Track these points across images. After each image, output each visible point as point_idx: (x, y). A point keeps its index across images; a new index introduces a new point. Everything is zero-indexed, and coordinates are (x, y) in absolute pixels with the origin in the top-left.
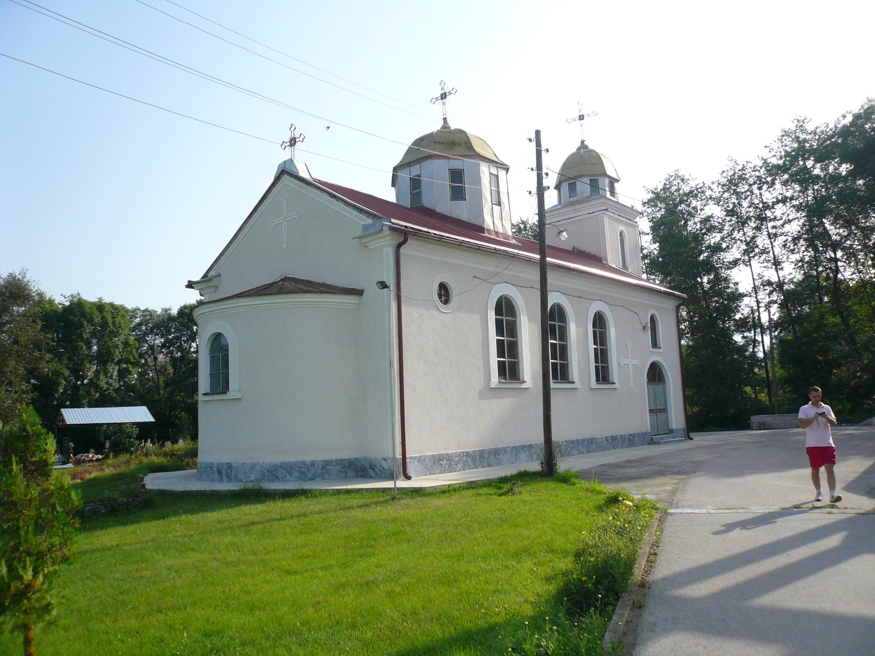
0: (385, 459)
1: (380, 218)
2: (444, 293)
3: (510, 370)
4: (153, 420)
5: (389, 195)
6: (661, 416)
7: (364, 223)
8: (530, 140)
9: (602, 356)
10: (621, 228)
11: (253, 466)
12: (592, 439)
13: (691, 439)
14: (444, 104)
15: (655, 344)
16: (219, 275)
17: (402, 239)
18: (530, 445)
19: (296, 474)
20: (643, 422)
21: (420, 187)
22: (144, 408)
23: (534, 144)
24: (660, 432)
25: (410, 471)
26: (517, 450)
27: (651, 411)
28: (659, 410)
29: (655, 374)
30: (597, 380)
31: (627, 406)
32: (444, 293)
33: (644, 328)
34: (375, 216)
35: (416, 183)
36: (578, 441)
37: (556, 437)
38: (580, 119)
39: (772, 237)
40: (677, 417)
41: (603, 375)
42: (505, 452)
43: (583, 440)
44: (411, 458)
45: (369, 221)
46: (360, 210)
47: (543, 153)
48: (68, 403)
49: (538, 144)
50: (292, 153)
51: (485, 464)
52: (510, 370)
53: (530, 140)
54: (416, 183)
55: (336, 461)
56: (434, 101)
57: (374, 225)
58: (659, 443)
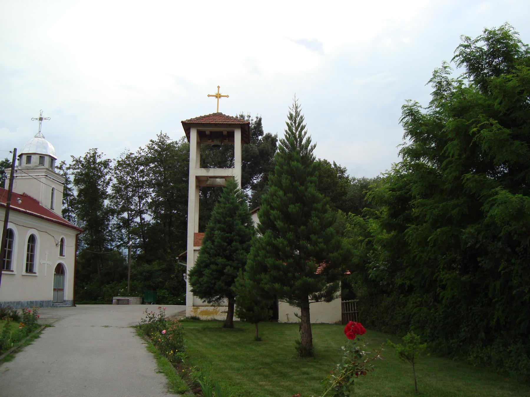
6: (60, 293)
9: (30, 258)
12: (19, 302)
15: (61, 254)
20: (49, 295)
23: (12, 155)
24: (57, 303)
27: (54, 290)
28: (59, 289)
29: (60, 270)
30: (27, 271)
33: (57, 245)
36: (11, 302)
38: (40, 120)
39: (141, 198)
40: (69, 293)
41: (30, 268)
43: (14, 302)
44: (314, 324)
48: (20, 202)
58: (57, 307)
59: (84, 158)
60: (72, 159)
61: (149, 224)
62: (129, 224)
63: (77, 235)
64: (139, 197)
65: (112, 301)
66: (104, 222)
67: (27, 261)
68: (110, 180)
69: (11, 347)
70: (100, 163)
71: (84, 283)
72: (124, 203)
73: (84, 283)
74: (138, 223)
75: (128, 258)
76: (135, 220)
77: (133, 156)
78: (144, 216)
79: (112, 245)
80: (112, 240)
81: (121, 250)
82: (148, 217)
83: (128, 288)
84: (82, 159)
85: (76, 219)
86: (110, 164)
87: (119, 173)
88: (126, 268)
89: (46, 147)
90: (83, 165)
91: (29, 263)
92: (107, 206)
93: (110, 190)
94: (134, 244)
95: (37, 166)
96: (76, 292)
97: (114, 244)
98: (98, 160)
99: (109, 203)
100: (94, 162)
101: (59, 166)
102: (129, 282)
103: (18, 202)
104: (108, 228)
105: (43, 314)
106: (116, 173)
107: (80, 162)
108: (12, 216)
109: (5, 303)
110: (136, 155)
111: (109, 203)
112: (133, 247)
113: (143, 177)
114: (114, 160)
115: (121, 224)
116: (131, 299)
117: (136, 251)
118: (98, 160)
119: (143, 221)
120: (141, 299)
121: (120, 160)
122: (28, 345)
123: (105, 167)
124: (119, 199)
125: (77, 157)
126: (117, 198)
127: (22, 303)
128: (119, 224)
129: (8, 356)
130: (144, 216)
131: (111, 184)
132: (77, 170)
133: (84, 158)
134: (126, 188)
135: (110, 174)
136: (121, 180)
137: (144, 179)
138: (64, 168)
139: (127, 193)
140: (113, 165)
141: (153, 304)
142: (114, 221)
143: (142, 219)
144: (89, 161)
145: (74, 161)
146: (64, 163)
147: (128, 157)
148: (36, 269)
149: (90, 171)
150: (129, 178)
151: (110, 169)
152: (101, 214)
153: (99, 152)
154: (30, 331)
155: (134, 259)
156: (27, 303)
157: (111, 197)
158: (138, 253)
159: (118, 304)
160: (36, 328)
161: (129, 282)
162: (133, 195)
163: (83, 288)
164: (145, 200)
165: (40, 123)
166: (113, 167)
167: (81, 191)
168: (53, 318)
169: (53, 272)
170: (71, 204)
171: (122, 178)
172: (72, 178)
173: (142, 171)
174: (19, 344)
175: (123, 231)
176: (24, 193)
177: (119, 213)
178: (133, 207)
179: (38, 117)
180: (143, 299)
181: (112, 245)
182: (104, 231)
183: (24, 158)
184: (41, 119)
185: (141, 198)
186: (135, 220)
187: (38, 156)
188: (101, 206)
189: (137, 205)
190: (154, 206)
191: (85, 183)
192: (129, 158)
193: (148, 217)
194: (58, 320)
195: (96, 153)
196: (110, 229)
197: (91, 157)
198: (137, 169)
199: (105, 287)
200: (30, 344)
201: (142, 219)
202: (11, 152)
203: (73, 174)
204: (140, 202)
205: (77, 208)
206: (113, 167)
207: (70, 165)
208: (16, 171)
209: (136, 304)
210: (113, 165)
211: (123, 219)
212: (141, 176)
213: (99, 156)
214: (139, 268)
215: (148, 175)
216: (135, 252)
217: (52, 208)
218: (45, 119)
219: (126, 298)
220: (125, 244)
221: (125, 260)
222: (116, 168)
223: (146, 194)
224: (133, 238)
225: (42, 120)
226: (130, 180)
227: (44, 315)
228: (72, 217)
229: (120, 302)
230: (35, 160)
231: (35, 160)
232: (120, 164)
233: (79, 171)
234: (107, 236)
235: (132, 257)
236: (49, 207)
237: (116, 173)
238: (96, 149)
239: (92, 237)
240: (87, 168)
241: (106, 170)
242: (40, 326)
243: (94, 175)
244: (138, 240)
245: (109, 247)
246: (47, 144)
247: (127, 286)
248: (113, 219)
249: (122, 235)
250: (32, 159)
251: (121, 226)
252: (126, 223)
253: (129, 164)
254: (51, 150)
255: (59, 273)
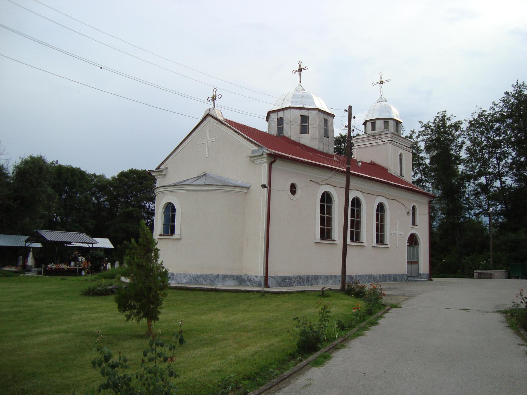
0: (256, 277)
1: (262, 147)
2: (293, 189)
3: (326, 234)
4: (113, 247)
5: (263, 126)
6: (414, 266)
7: (253, 149)
8: (346, 111)
10: (401, 151)
11: (185, 275)
13: (432, 280)
14: (300, 75)
15: (414, 223)
16: (167, 169)
17: (273, 160)
18: (335, 276)
19: (208, 281)
20: (402, 268)
21: (282, 124)
22: (107, 239)
23: (347, 113)
24: (412, 276)
25: (270, 283)
26: (327, 278)
27: (408, 262)
28: (413, 261)
29: (413, 240)
30: (377, 242)
31: (392, 259)
32: (293, 189)
33: (408, 213)
34: (259, 146)
35: (281, 121)
36: (363, 275)
37: (348, 273)
39: (499, 159)
40: (424, 266)
41: (380, 239)
42: (321, 278)
44: (270, 277)
45: (256, 148)
46: (251, 142)
47: (352, 119)
49: (350, 114)
50: (214, 105)
51: (309, 284)
52: (326, 234)
53: (346, 111)
54: (281, 121)
55: (230, 275)
56: (294, 72)
57: (258, 150)
58: (411, 281)
59: (433, 123)
60: (420, 125)
61: (511, 188)
62: (488, 189)
63: (430, 203)
64: (497, 159)
65: (473, 275)
66: (460, 189)
67: (377, 231)
68: (463, 143)
69: (335, 339)
70: (451, 126)
71: (442, 255)
72: (481, 167)
73: (442, 255)
74: (497, 187)
75: (489, 227)
76: (494, 185)
77: (486, 113)
78: (505, 179)
79: (470, 214)
80: (471, 208)
81: (480, 219)
82: (509, 181)
83: (491, 260)
84: (431, 124)
85: (430, 189)
86: (462, 126)
87: (472, 134)
88: (487, 238)
89: (389, 110)
90: (432, 130)
91: (379, 233)
92: (462, 172)
93: (463, 154)
94: (495, 210)
95: (382, 132)
96: (432, 264)
97: (472, 212)
98: (448, 123)
99: (464, 168)
100: (444, 125)
101: (409, 136)
102: (491, 253)
103: (357, 165)
104: (464, 195)
105: (390, 289)
106: (468, 135)
107: (430, 127)
108: (353, 182)
109: (356, 276)
110: (489, 112)
111: (464, 168)
112: (494, 214)
113: (501, 136)
114: (465, 120)
115: (479, 190)
116: (495, 272)
117: (498, 218)
118: (448, 123)
119: (504, 185)
120: (507, 273)
121: (472, 119)
122: (358, 335)
123: (457, 130)
124: (475, 162)
125: (425, 122)
126: (472, 162)
127: (374, 276)
128: (477, 190)
129: (321, 356)
130: (505, 179)
131: (464, 147)
132: (427, 136)
133: (433, 123)
134: (482, 149)
135: (462, 136)
136: (474, 141)
137: (501, 138)
138: (414, 137)
139: (482, 155)
140: (464, 126)
141: (522, 278)
142: (470, 187)
143: (502, 183)
144: (438, 125)
145: (422, 127)
146: (413, 132)
147: (480, 116)
148: (387, 240)
149: (441, 134)
150: (483, 139)
151: (462, 131)
152: (456, 181)
153: (448, 115)
154: (370, 312)
155: (496, 227)
156: (380, 276)
157: (466, 162)
158: (500, 220)
159: (480, 277)
160: (380, 308)
161: (491, 253)
162: (490, 157)
163: (441, 260)
164: (504, 161)
165: (381, 87)
166: (465, 129)
167: (432, 159)
168: (404, 296)
169: (406, 243)
170: (424, 172)
171: (475, 139)
172: (422, 145)
173: (498, 129)
174: (349, 333)
175: (482, 197)
176: (372, 161)
177: (476, 178)
178: (491, 170)
179: (378, 81)
180: (509, 273)
181: (470, 214)
182: (461, 198)
183: (369, 124)
184: (381, 83)
185: (499, 159)
186: (494, 185)
187: (382, 121)
188: (454, 173)
189: (495, 167)
190: (517, 167)
191: (436, 148)
192: (482, 116)
193: (509, 181)
194: (409, 297)
195: (445, 116)
196: (467, 196)
197: (440, 121)
198: (492, 127)
199: (465, 259)
200: (361, 335)
201: (502, 183)
202: (346, 127)
203: (423, 141)
204: (498, 164)
205: (431, 177)
206: (465, 129)
207: (419, 132)
208: (353, 130)
209: (501, 278)
210: (464, 126)
211: (480, 185)
212: (497, 135)
213: (449, 119)
214: (502, 237)
215: (505, 132)
216: (497, 220)
217: (401, 175)
218: (386, 81)
219: (489, 271)
220: (485, 212)
221: (486, 229)
222: (468, 129)
223: (505, 155)
224: (493, 205)
225: (380, 82)
226: (484, 140)
227: (389, 291)
228: (426, 187)
229: (482, 276)
230: (379, 125)
231: (379, 125)
232: (473, 124)
233: (429, 136)
234: (465, 204)
235: (493, 226)
236: (398, 174)
237: (468, 135)
238: (445, 111)
239: (449, 206)
240: (436, 132)
241: (457, 133)
242: (384, 305)
243: (445, 139)
244: (500, 206)
245: (468, 216)
246: (390, 107)
247: (489, 258)
248: (469, 185)
249: (481, 202)
250: (376, 125)
251: (479, 193)
252: (485, 188)
253: (482, 123)
254: (395, 114)
255: (412, 244)
